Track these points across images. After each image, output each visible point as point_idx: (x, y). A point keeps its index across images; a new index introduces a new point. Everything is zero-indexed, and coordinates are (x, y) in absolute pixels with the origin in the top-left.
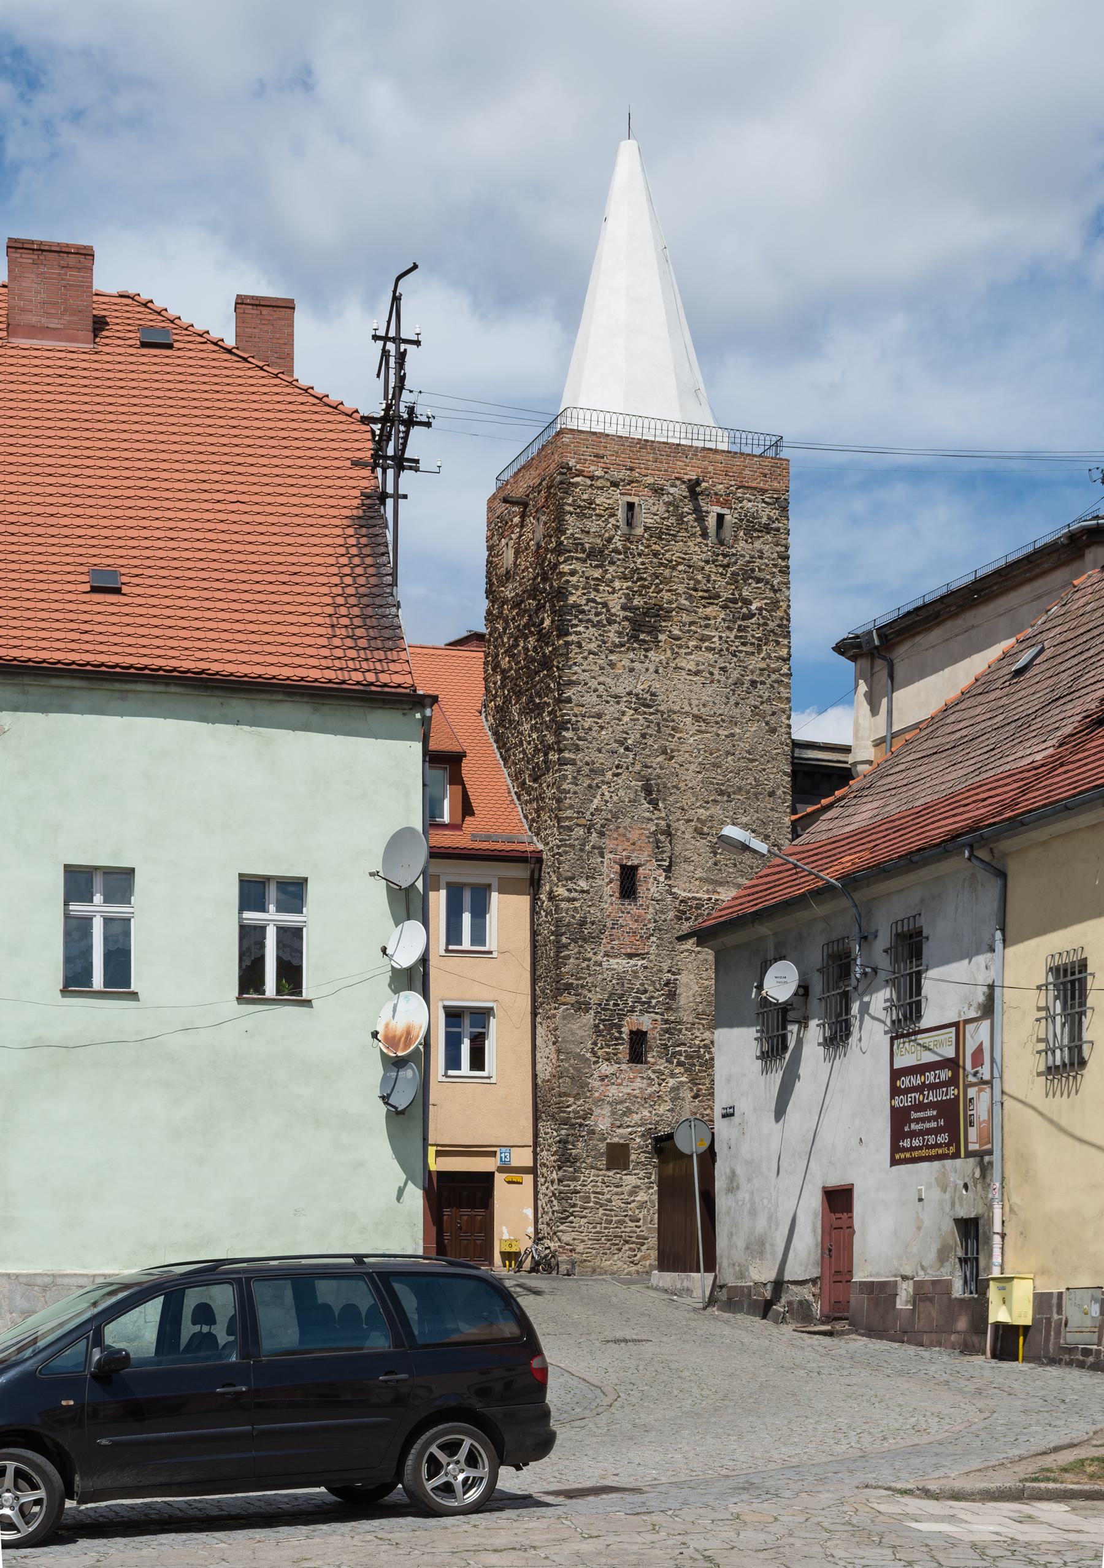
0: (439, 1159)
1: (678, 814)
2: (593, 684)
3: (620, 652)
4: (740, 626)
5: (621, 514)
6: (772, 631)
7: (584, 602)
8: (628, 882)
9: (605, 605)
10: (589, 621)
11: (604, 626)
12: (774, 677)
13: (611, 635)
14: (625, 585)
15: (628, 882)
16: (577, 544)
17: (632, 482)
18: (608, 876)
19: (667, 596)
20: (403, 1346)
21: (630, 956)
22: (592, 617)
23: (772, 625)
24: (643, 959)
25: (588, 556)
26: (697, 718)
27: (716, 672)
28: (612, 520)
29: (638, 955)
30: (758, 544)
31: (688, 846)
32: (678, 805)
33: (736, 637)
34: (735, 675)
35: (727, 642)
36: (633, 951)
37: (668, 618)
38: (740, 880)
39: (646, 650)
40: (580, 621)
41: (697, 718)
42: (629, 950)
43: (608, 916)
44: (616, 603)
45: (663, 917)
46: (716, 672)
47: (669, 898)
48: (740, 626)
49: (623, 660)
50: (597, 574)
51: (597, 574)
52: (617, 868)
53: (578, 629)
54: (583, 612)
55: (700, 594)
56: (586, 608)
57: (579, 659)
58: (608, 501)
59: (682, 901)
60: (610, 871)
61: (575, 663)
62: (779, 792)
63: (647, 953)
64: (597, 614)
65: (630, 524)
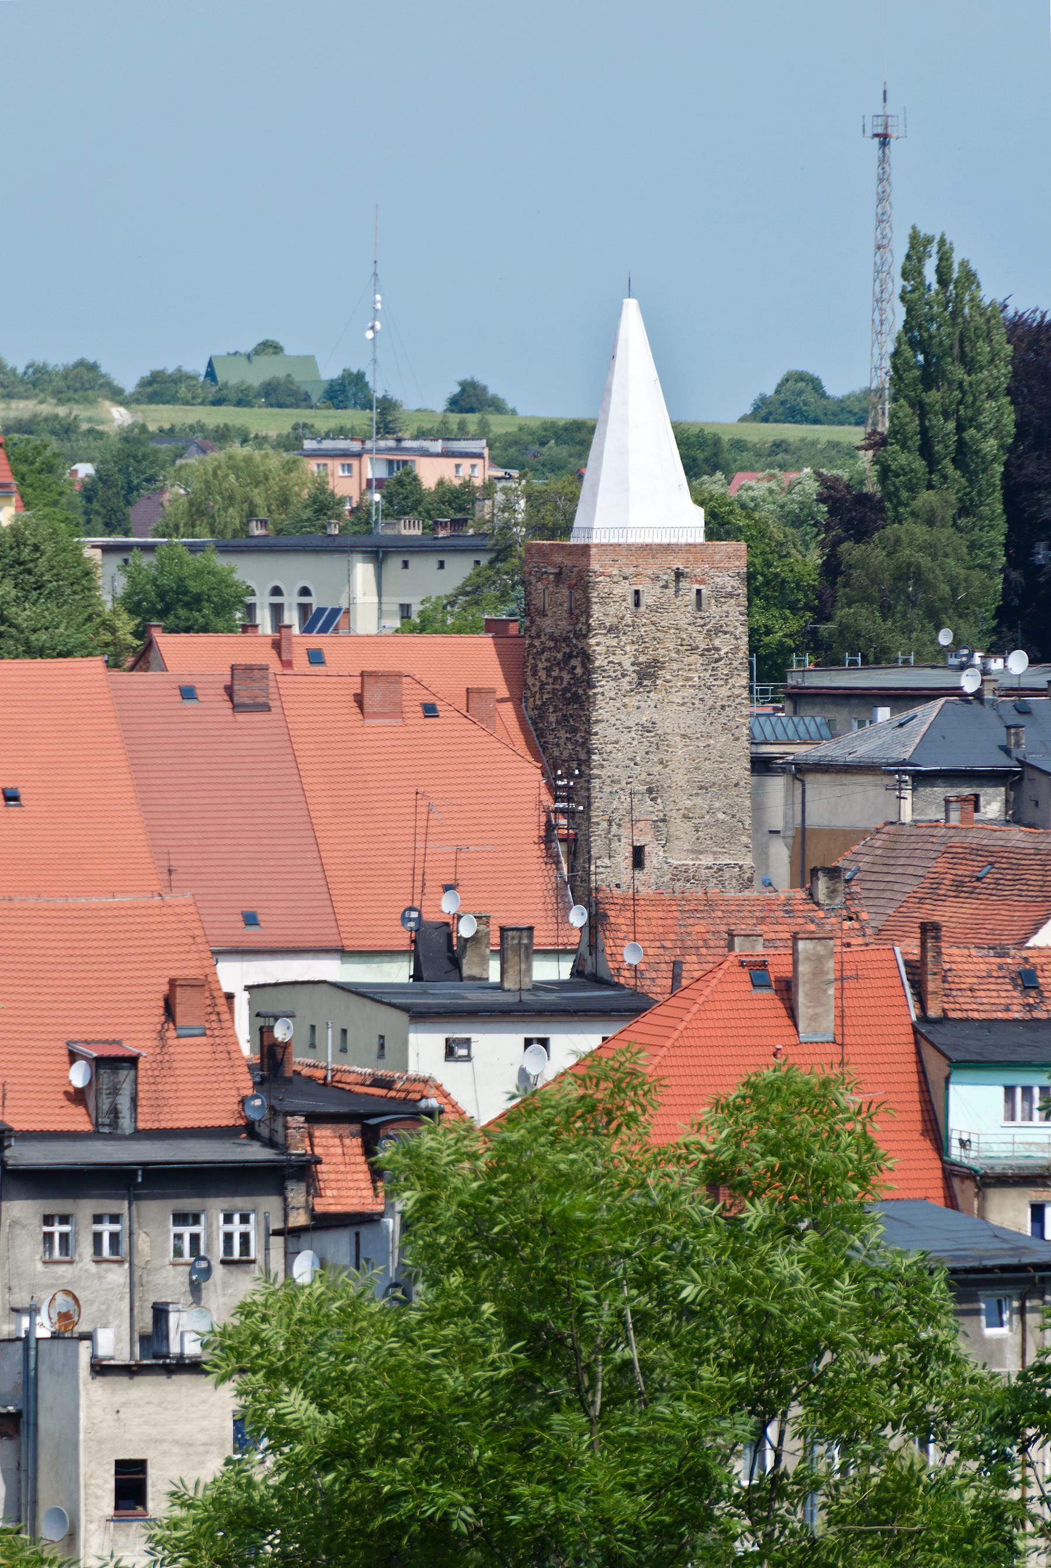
1: (672, 806)
2: (613, 720)
12: (737, 701)
19: (661, 652)
23: (736, 664)
26: (684, 736)
27: (697, 702)
34: (710, 703)
38: (715, 849)
41: (684, 736)
44: (627, 664)
46: (697, 702)
47: (666, 866)
49: (632, 701)
51: (614, 642)
52: (630, 848)
62: (742, 783)
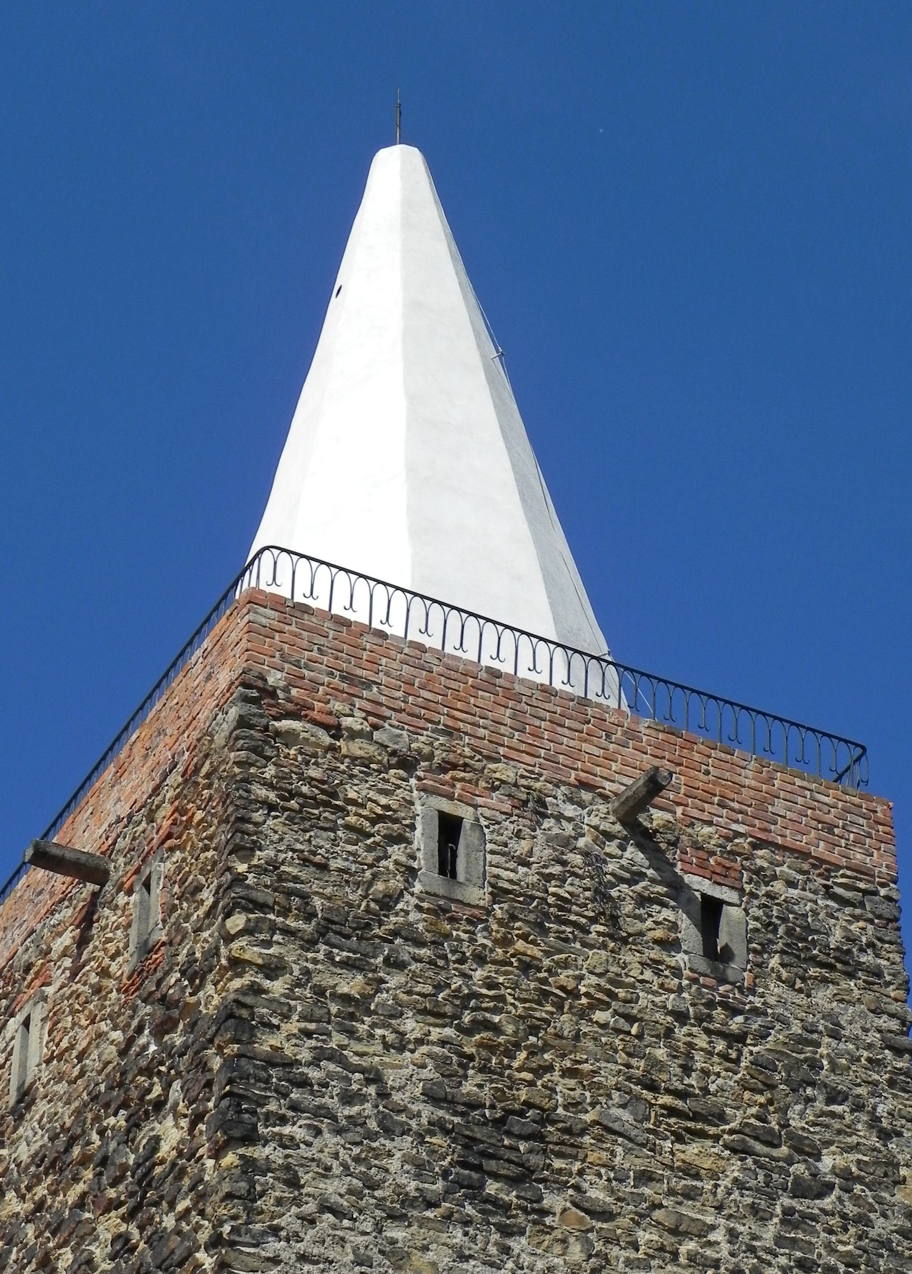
3: (423, 1223)
4: (788, 1212)
5: (424, 840)
6: (885, 1244)
7: (305, 1055)
9: (374, 1077)
10: (321, 1112)
11: (372, 1136)
13: (394, 1164)
14: (436, 1033)
16: (289, 893)
17: (454, 767)
19: (564, 1085)
22: (332, 1103)
25: (322, 932)
28: (397, 852)
30: (822, 997)
33: (779, 1240)
35: (752, 1250)
37: (570, 1151)
39: (506, 1231)
40: (295, 1107)
44: (409, 1076)
48: (788, 1212)
50: (351, 984)
53: (287, 1130)
54: (304, 1083)
55: (666, 1099)
56: (314, 1074)
57: (288, 1220)
58: (383, 801)
61: (275, 1231)
64: (348, 1098)
65: (447, 866)
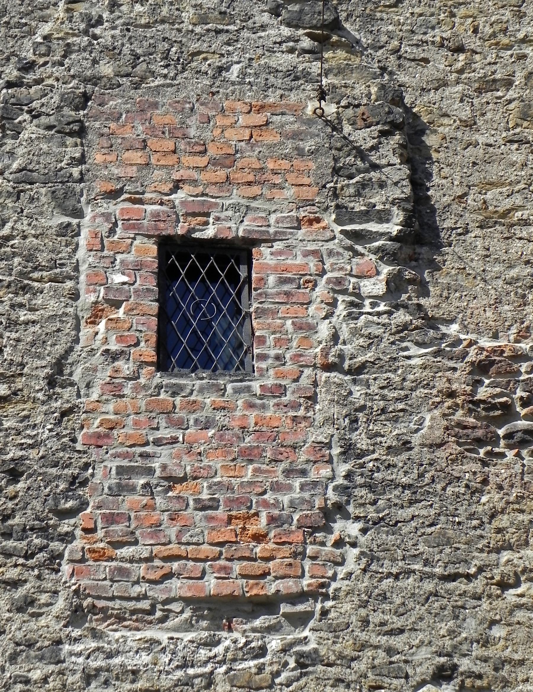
0: (93, 526)
8: (201, 293)
15: (201, 293)
18: (99, 280)
20: (195, 364)
21: (219, 611)
24: (300, 620)
29: (267, 605)
31: (494, 171)
32: (437, 34)
36: (237, 586)
42: (211, 585)
43: (99, 441)
45: (391, 433)
59: (482, 368)
60: (114, 269)
63: (318, 593)
